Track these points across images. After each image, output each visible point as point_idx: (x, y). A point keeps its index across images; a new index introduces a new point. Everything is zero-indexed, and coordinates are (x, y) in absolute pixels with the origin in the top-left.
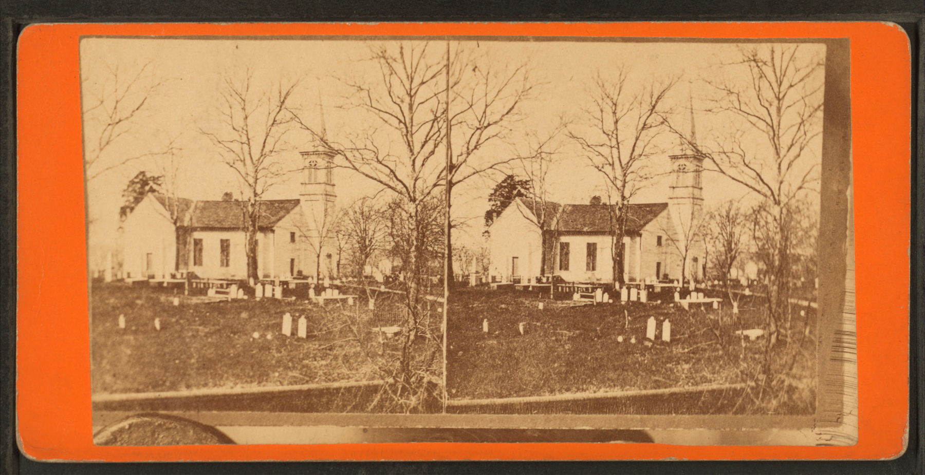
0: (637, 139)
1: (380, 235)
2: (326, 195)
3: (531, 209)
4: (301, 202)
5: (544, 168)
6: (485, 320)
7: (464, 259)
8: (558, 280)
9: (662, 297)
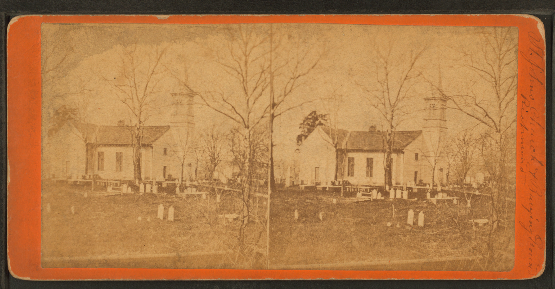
4: (423, 133)
6: (161, 205)
9: (418, 195)
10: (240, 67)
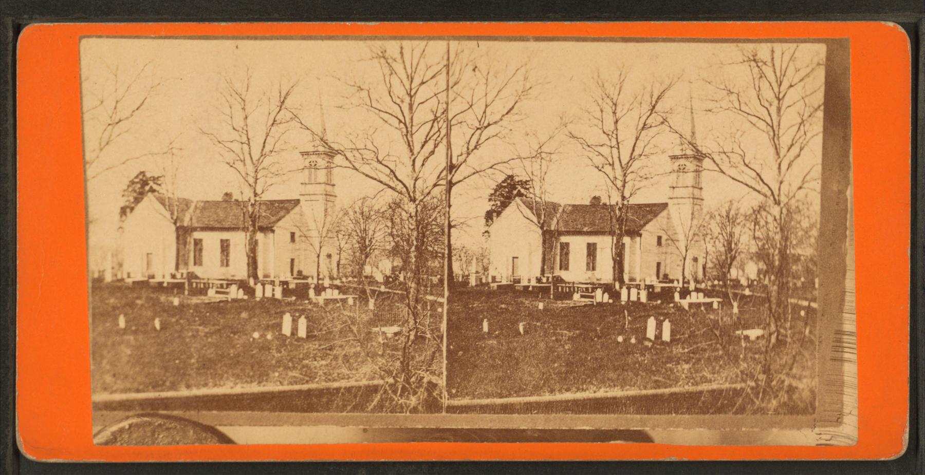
0: (637, 139)
1: (380, 235)
2: (326, 195)
3: (531, 209)
5: (544, 168)
6: (485, 320)
7: (464, 259)
8: (558, 280)
9: (662, 297)
10: (770, 115)
